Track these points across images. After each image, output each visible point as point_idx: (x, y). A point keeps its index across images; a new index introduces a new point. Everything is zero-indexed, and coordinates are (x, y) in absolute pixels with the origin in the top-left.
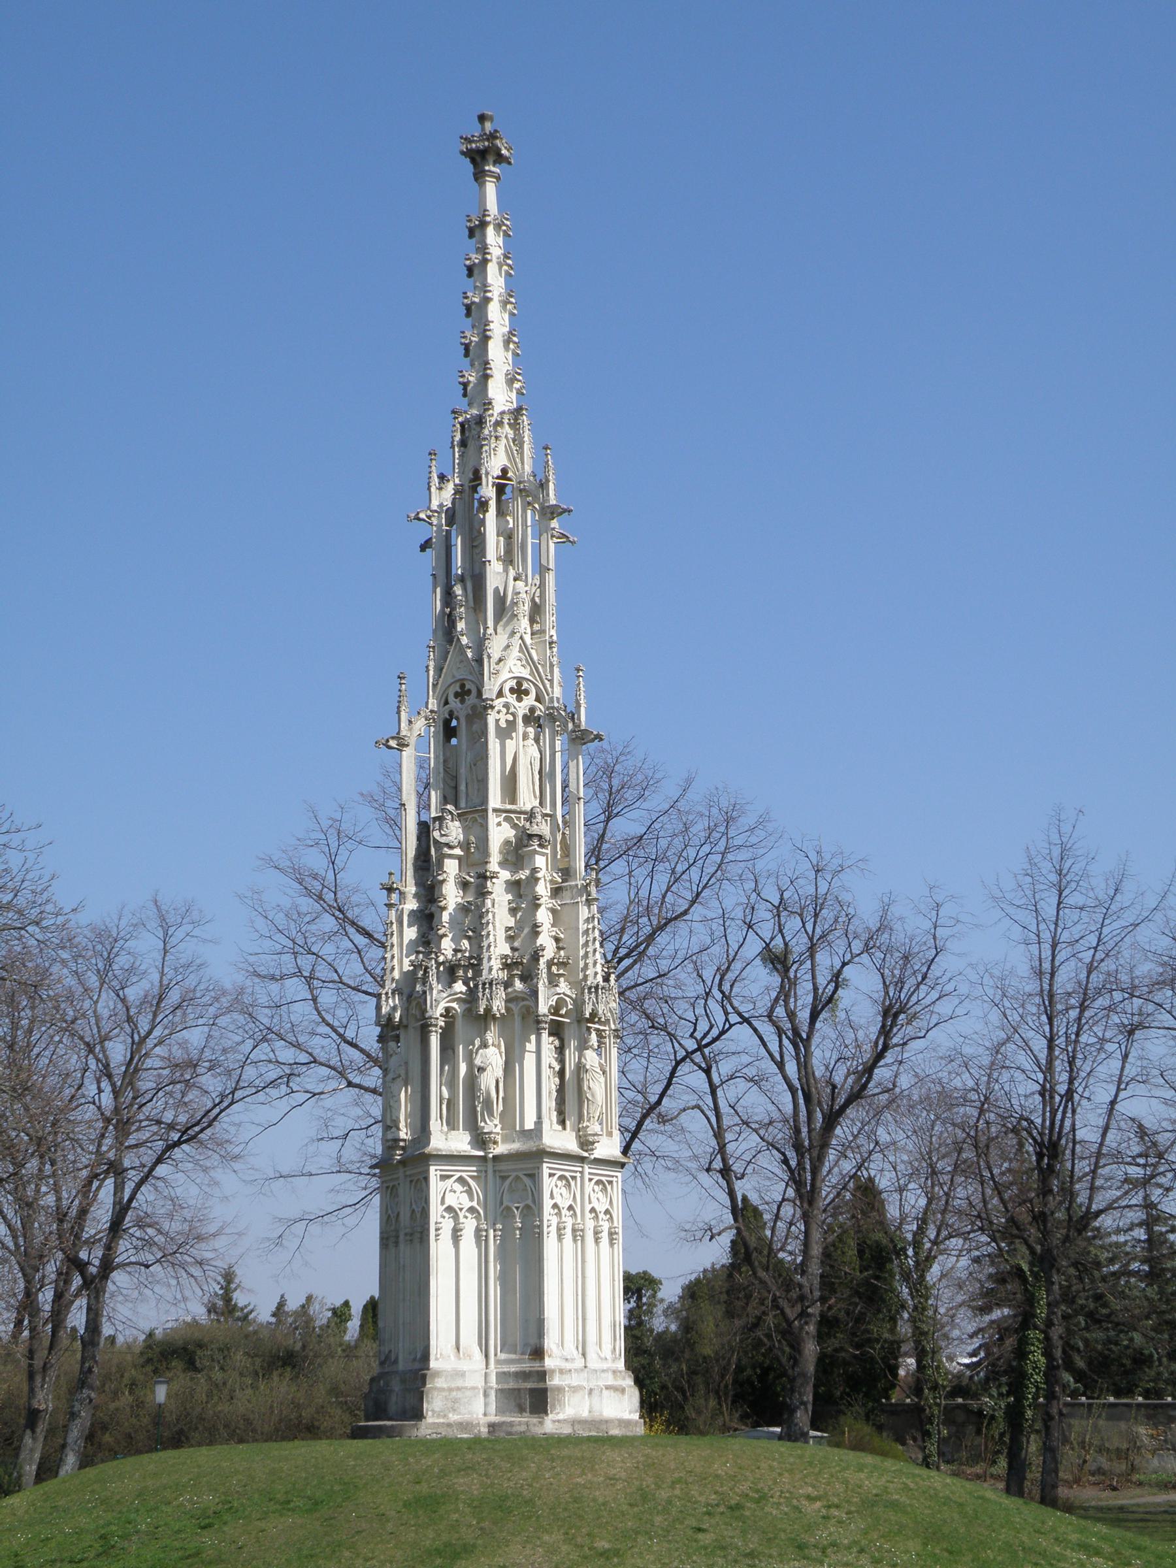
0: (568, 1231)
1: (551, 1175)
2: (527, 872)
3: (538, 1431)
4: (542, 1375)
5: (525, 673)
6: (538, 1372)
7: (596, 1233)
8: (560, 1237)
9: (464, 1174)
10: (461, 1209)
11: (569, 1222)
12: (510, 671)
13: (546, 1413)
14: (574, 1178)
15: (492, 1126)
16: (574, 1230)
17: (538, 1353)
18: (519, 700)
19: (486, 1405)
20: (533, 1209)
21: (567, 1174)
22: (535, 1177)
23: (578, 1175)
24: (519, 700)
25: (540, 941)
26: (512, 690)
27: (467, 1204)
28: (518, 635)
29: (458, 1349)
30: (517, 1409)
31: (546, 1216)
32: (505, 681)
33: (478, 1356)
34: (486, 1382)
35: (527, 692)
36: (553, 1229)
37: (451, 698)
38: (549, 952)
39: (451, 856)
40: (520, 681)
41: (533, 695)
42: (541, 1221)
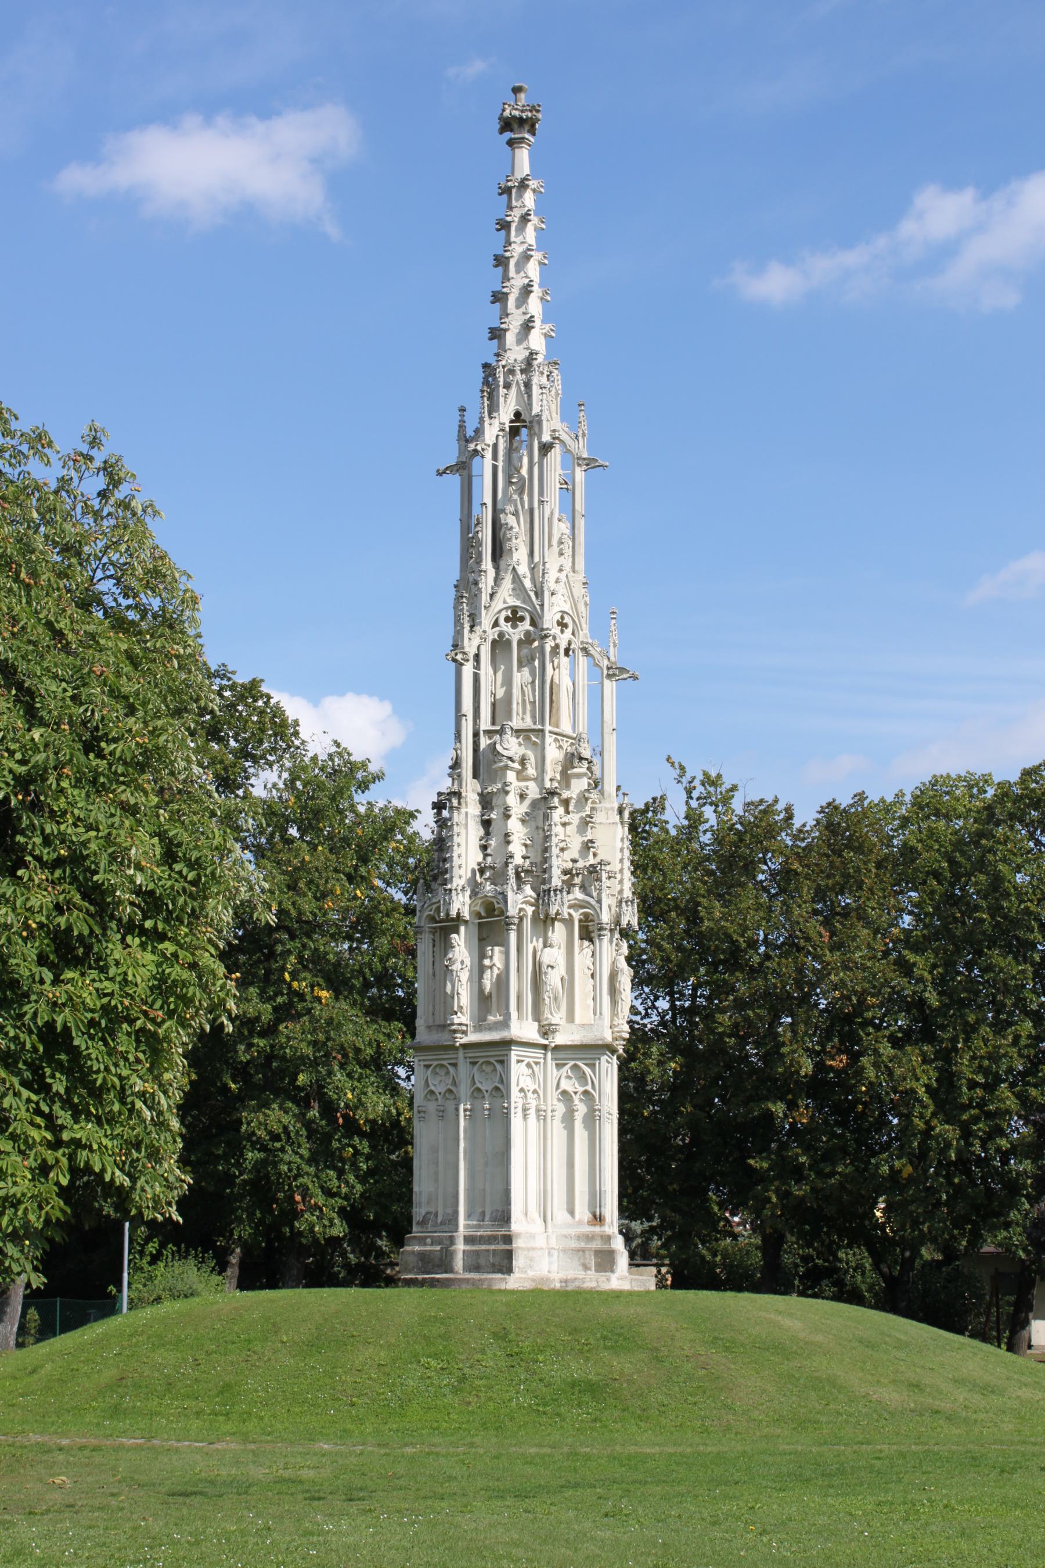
0: (532, 1112)
1: (518, 1061)
2: (499, 786)
3: (605, 1286)
4: (508, 1239)
5: (567, 608)
6: (505, 1236)
7: (525, 1110)
8: (525, 1116)
9: (531, 1060)
10: (576, 1093)
11: (533, 1104)
12: (505, 602)
13: (612, 1271)
14: (537, 1063)
15: (557, 1017)
16: (538, 1111)
17: (504, 1217)
18: (514, 626)
19: (550, 1263)
20: (501, 1091)
21: (445, 1063)
22: (504, 1062)
23: (542, 1061)
24: (514, 626)
25: (511, 848)
26: (507, 619)
27: (532, 1087)
28: (511, 568)
29: (526, 1214)
30: (581, 1268)
31: (513, 1099)
32: (500, 611)
33: (540, 1222)
34: (548, 1243)
35: (522, 619)
36: (519, 1110)
37: (502, 621)
38: (518, 860)
39: (512, 769)
40: (514, 610)
41: (528, 621)
42: (509, 1103)
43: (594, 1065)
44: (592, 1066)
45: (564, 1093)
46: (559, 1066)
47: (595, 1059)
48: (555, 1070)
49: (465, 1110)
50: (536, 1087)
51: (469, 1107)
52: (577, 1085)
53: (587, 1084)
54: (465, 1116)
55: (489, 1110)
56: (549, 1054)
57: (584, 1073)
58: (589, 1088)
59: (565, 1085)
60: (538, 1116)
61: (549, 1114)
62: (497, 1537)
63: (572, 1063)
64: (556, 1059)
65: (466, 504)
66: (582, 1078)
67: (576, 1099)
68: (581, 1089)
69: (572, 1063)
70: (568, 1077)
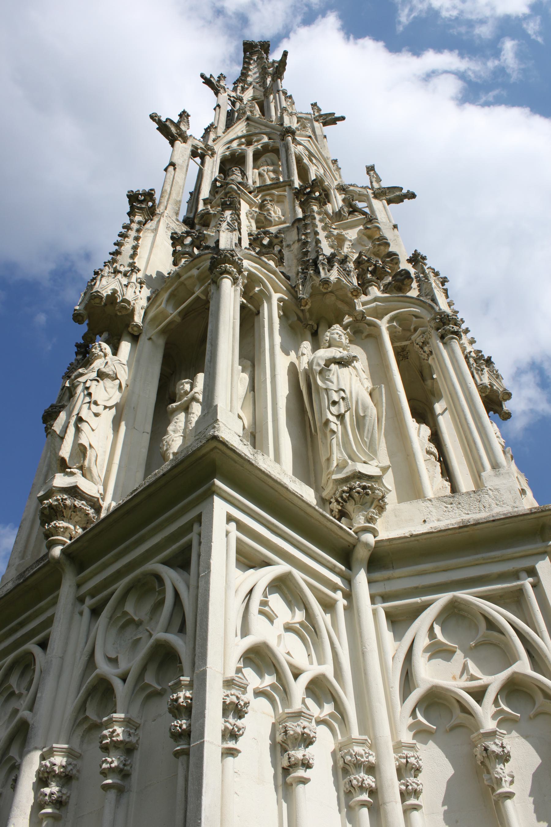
10: (479, 694)
20: (172, 661)
43: (520, 592)
44: (515, 601)
45: (436, 702)
46: (399, 621)
47: (515, 575)
48: (388, 635)
49: (43, 780)
50: (328, 670)
51: (59, 760)
52: (473, 669)
53: (510, 658)
54: (38, 805)
55: (128, 749)
56: (361, 578)
57: (491, 624)
58: (523, 666)
59: (430, 673)
60: (347, 794)
61: (393, 786)
62: (327, 390)
63: (444, 598)
64: (385, 598)
65: (257, 517)
66: (490, 644)
67: (486, 715)
68: (495, 681)
69: (444, 598)
70: (437, 651)
